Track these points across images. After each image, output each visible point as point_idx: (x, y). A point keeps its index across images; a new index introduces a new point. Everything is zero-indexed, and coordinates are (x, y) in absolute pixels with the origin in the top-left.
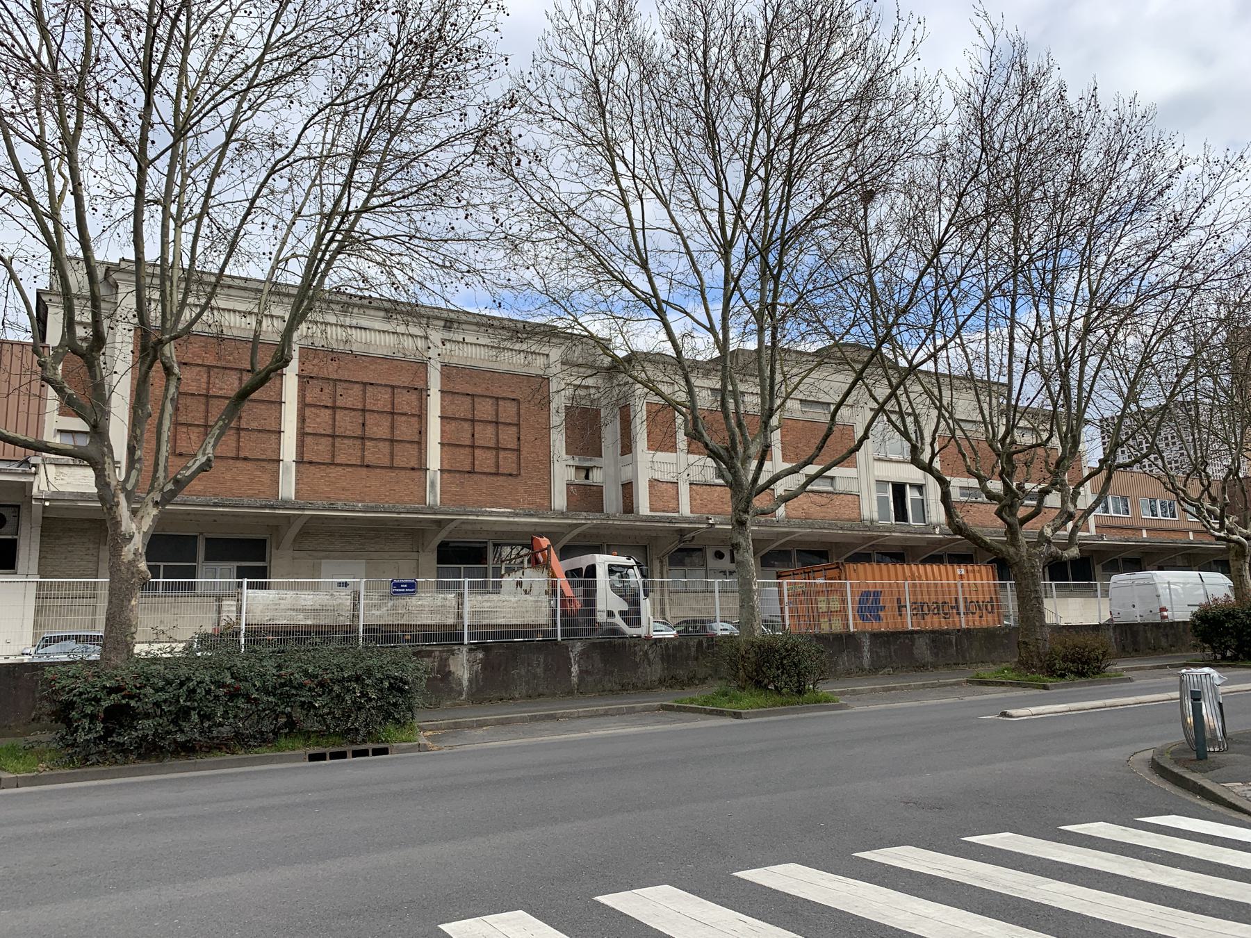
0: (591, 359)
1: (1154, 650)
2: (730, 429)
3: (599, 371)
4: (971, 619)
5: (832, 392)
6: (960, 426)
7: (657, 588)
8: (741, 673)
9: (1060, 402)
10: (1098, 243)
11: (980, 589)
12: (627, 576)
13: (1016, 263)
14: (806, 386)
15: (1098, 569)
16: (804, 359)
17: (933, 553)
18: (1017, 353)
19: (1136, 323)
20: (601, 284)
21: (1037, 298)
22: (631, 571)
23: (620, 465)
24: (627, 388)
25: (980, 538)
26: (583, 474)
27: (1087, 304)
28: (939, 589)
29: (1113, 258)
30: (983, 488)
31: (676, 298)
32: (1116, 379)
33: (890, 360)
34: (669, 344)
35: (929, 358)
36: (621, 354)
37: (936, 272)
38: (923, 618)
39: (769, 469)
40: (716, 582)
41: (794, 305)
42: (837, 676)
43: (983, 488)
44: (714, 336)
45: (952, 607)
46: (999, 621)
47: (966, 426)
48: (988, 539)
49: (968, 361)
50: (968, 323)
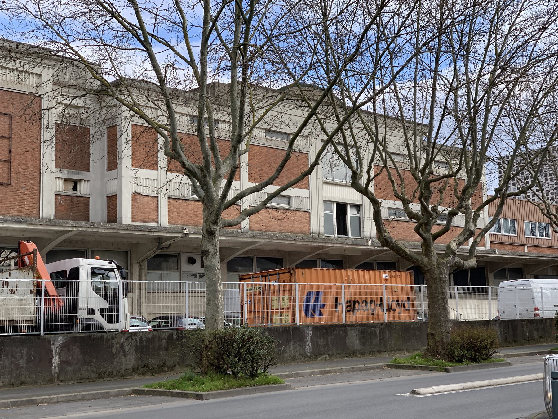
0: (81, 81)
1: (528, 340)
2: (204, 151)
3: (88, 93)
5: (291, 124)
6: (391, 158)
7: (136, 289)
8: (205, 361)
9: (469, 142)
10: (504, 14)
11: (400, 291)
12: (108, 277)
13: (442, 25)
14: (271, 117)
15: (491, 276)
16: (269, 94)
17: (365, 261)
18: (438, 100)
19: (528, 81)
20: (93, 13)
21: (455, 56)
22: (112, 273)
23: (106, 179)
24: (114, 110)
25: (402, 250)
26: (71, 186)
27: (493, 63)
28: (369, 290)
29: (514, 28)
30: (406, 209)
31: (160, 32)
32: (512, 125)
33: (339, 100)
34: (153, 73)
35: (369, 100)
36: (110, 79)
37: (378, 28)
38: (355, 314)
39: (237, 187)
40: (187, 284)
41: (262, 47)
42: (284, 362)
43: (406, 209)
44: (193, 68)
45: (378, 305)
46: (414, 316)
47: (396, 159)
48: (408, 250)
49: (400, 104)
50: (401, 73)
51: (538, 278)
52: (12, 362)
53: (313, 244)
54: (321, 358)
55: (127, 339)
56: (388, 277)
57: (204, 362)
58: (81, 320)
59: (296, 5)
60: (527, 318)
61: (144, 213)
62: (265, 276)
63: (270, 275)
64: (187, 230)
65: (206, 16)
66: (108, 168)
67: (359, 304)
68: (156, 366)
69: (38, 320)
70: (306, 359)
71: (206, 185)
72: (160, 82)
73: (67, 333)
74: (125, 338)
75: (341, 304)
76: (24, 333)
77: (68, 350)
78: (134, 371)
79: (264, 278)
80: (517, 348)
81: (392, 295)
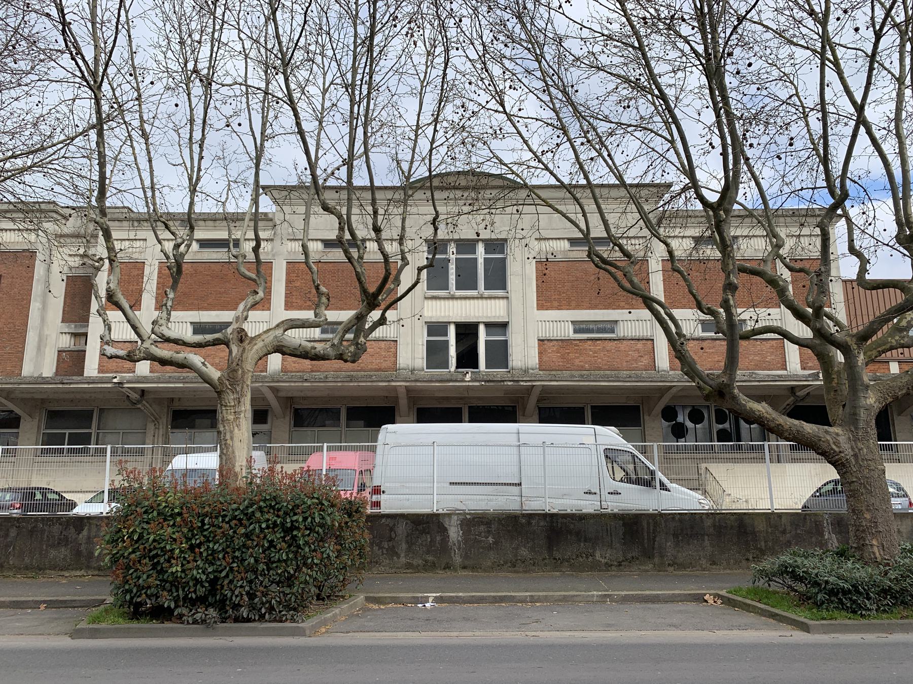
59: (880, 64)
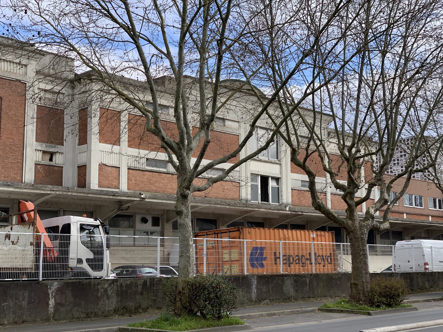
4: (318, 267)
8: (178, 304)
11: (324, 247)
17: (282, 223)
22: (96, 230)
23: (77, 152)
26: (48, 157)
45: (307, 259)
51: (439, 240)
52: (16, 303)
53: (243, 208)
54: (263, 303)
55: (110, 285)
56: (315, 236)
57: (178, 305)
58: (71, 268)
60: (421, 271)
61: (108, 180)
62: (217, 234)
63: (221, 233)
64: (144, 195)
65: (184, 17)
66: (79, 143)
67: (293, 258)
68: (133, 308)
69: (37, 267)
70: (252, 303)
71: (181, 156)
72: (145, 70)
73: (60, 279)
74: (108, 284)
75: (279, 258)
76: (26, 279)
77: (62, 293)
78: (115, 312)
79: (216, 235)
80: (415, 296)
81: (318, 251)
